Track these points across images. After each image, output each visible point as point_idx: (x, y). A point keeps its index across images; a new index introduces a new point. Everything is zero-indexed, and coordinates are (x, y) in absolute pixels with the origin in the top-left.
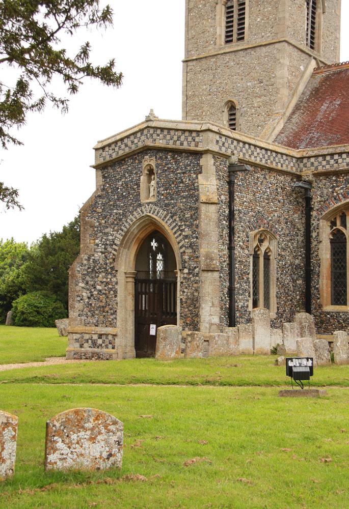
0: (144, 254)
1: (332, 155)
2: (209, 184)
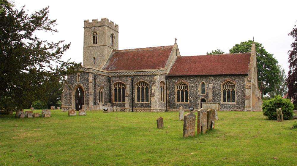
0: (77, 92)
1: (115, 72)
2: (91, 79)
